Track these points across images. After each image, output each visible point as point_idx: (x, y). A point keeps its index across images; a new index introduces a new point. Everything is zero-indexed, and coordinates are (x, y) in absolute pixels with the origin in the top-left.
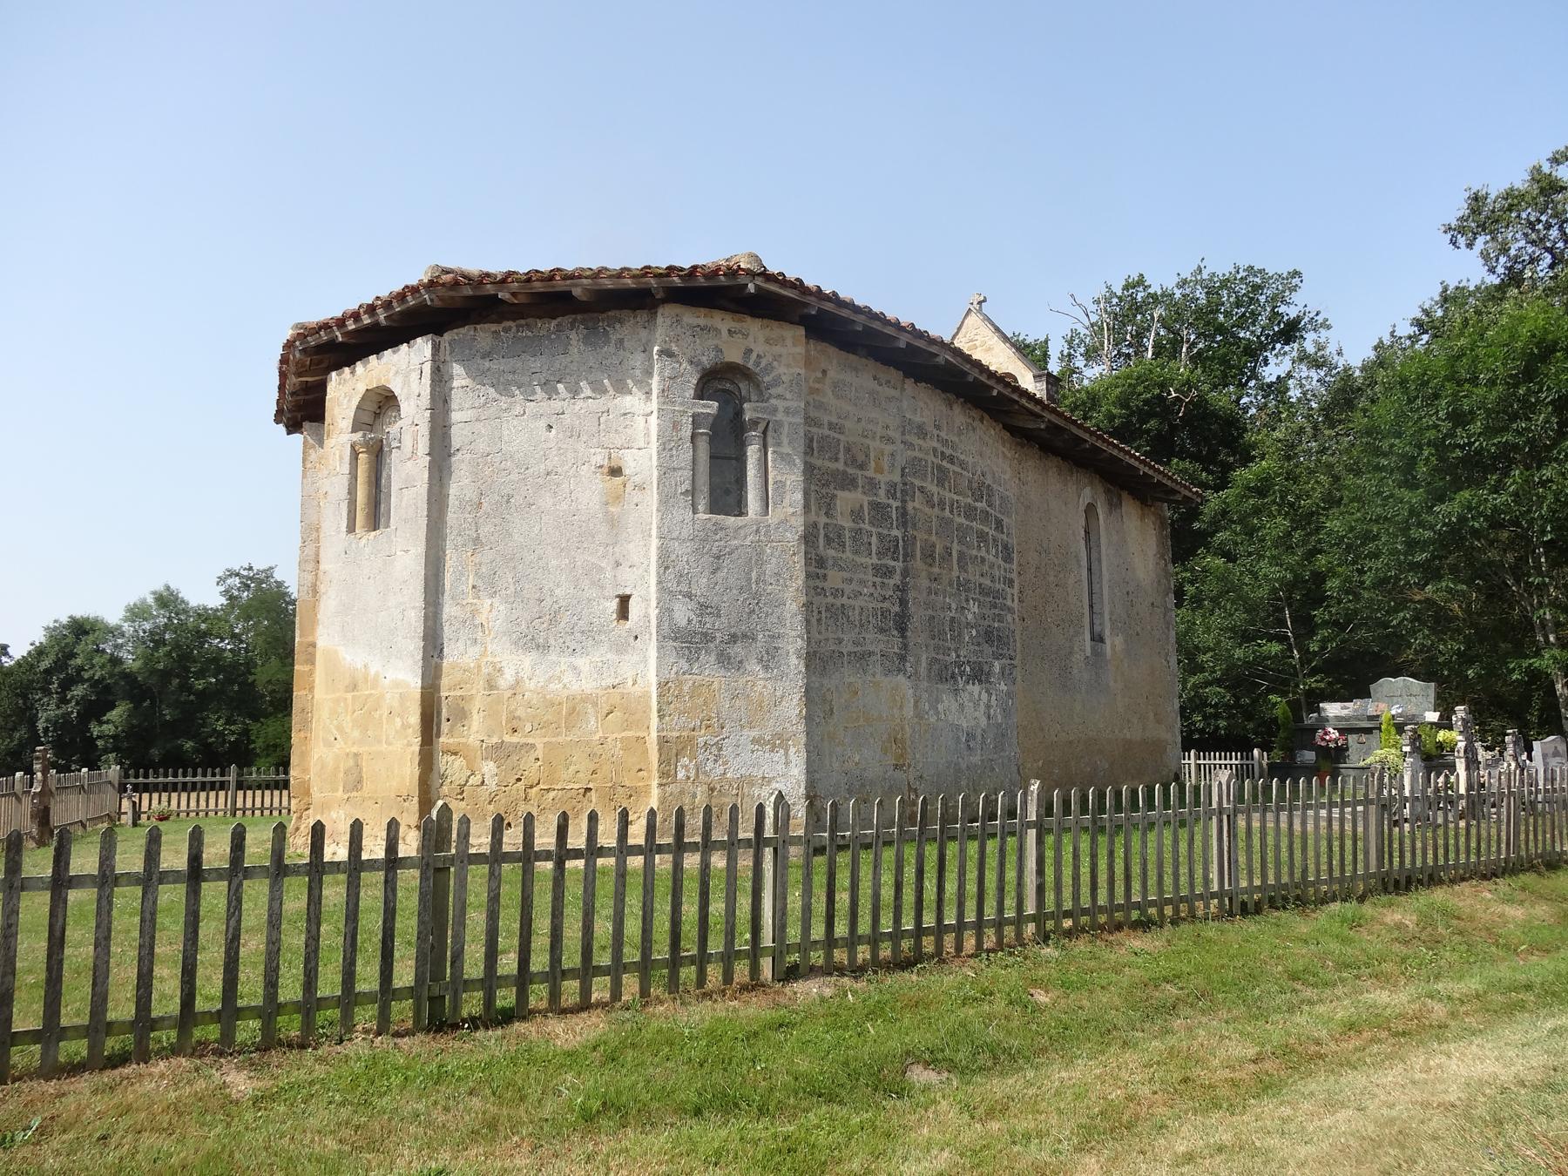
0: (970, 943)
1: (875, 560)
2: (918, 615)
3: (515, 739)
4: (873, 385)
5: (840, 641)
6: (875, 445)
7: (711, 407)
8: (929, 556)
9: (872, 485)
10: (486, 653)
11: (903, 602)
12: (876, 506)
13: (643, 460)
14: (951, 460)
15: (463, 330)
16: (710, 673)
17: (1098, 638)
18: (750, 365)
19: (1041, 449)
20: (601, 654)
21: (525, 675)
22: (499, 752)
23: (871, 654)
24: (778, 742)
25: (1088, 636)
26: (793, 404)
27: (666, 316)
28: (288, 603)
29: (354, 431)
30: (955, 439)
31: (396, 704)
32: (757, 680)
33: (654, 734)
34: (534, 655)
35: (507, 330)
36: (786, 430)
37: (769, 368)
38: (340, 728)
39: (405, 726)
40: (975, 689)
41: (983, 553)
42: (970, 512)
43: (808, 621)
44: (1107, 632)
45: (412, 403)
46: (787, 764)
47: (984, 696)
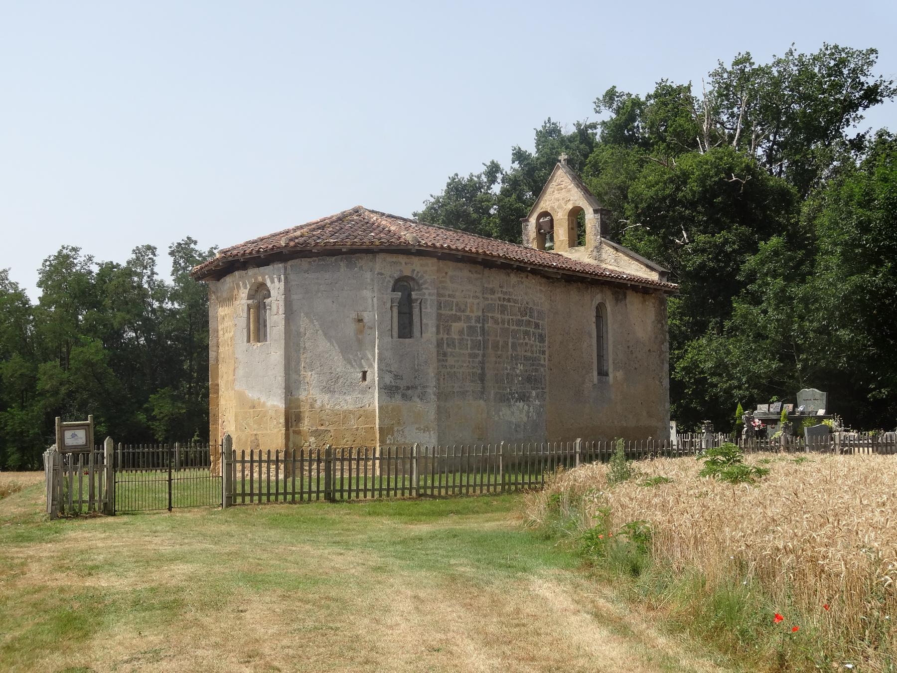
0: (478, 492)
1: (469, 351)
2: (489, 374)
3: (322, 428)
4: (470, 275)
5: (453, 387)
6: (470, 301)
7: (399, 294)
8: (496, 346)
9: (468, 318)
10: (313, 394)
11: (483, 368)
12: (470, 328)
13: (371, 316)
14: (509, 300)
15: (297, 261)
16: (397, 401)
17: (603, 373)
18: (414, 276)
19: (566, 281)
20: (356, 395)
21: (326, 403)
22: (317, 433)
23: (467, 391)
24: (426, 429)
25: (595, 373)
26: (432, 291)
27: (380, 257)
28: (13, 301)
29: (248, 299)
30: (511, 290)
31: (273, 414)
32: (419, 405)
33: (377, 426)
34: (329, 395)
35: (314, 261)
36: (428, 302)
37: (422, 277)
38: (248, 424)
39: (278, 423)
40: (521, 404)
41: (527, 340)
42: (519, 323)
43: (439, 380)
44: (610, 370)
45: (276, 291)
46: (430, 437)
47: (526, 407)
